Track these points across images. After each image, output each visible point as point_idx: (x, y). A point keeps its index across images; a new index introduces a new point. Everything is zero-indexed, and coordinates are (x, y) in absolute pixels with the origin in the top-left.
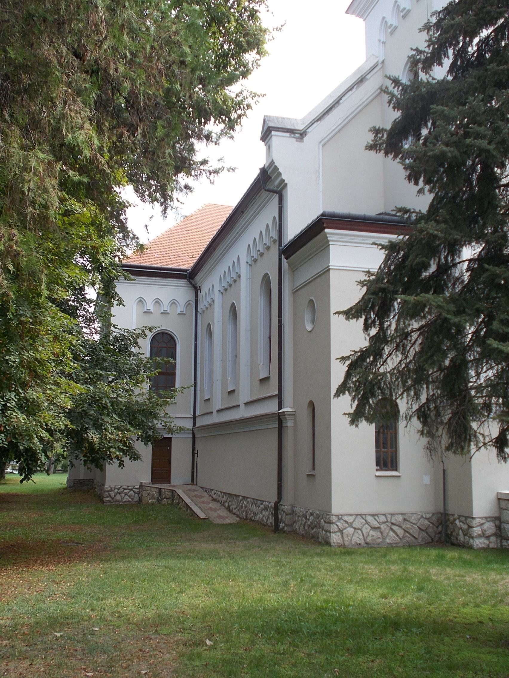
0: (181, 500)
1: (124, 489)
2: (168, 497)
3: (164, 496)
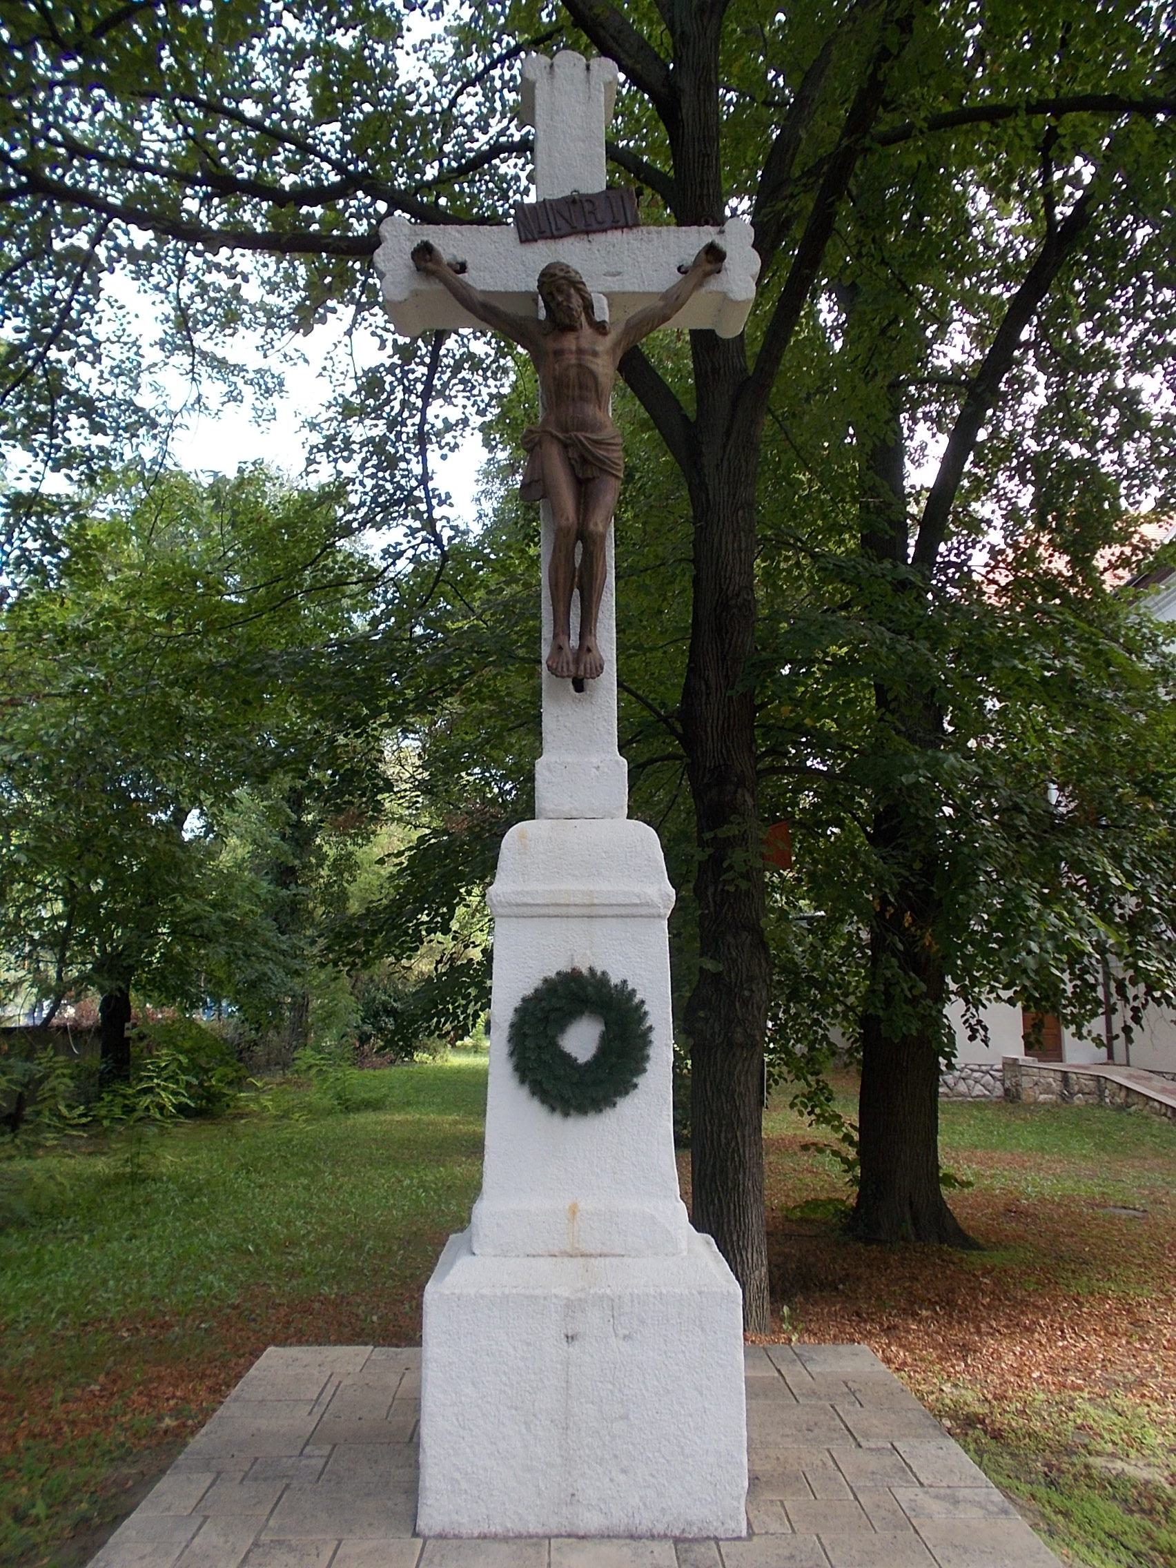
0: (1134, 1098)
1: (973, 1070)
2: (1087, 1090)
3: (1076, 1088)
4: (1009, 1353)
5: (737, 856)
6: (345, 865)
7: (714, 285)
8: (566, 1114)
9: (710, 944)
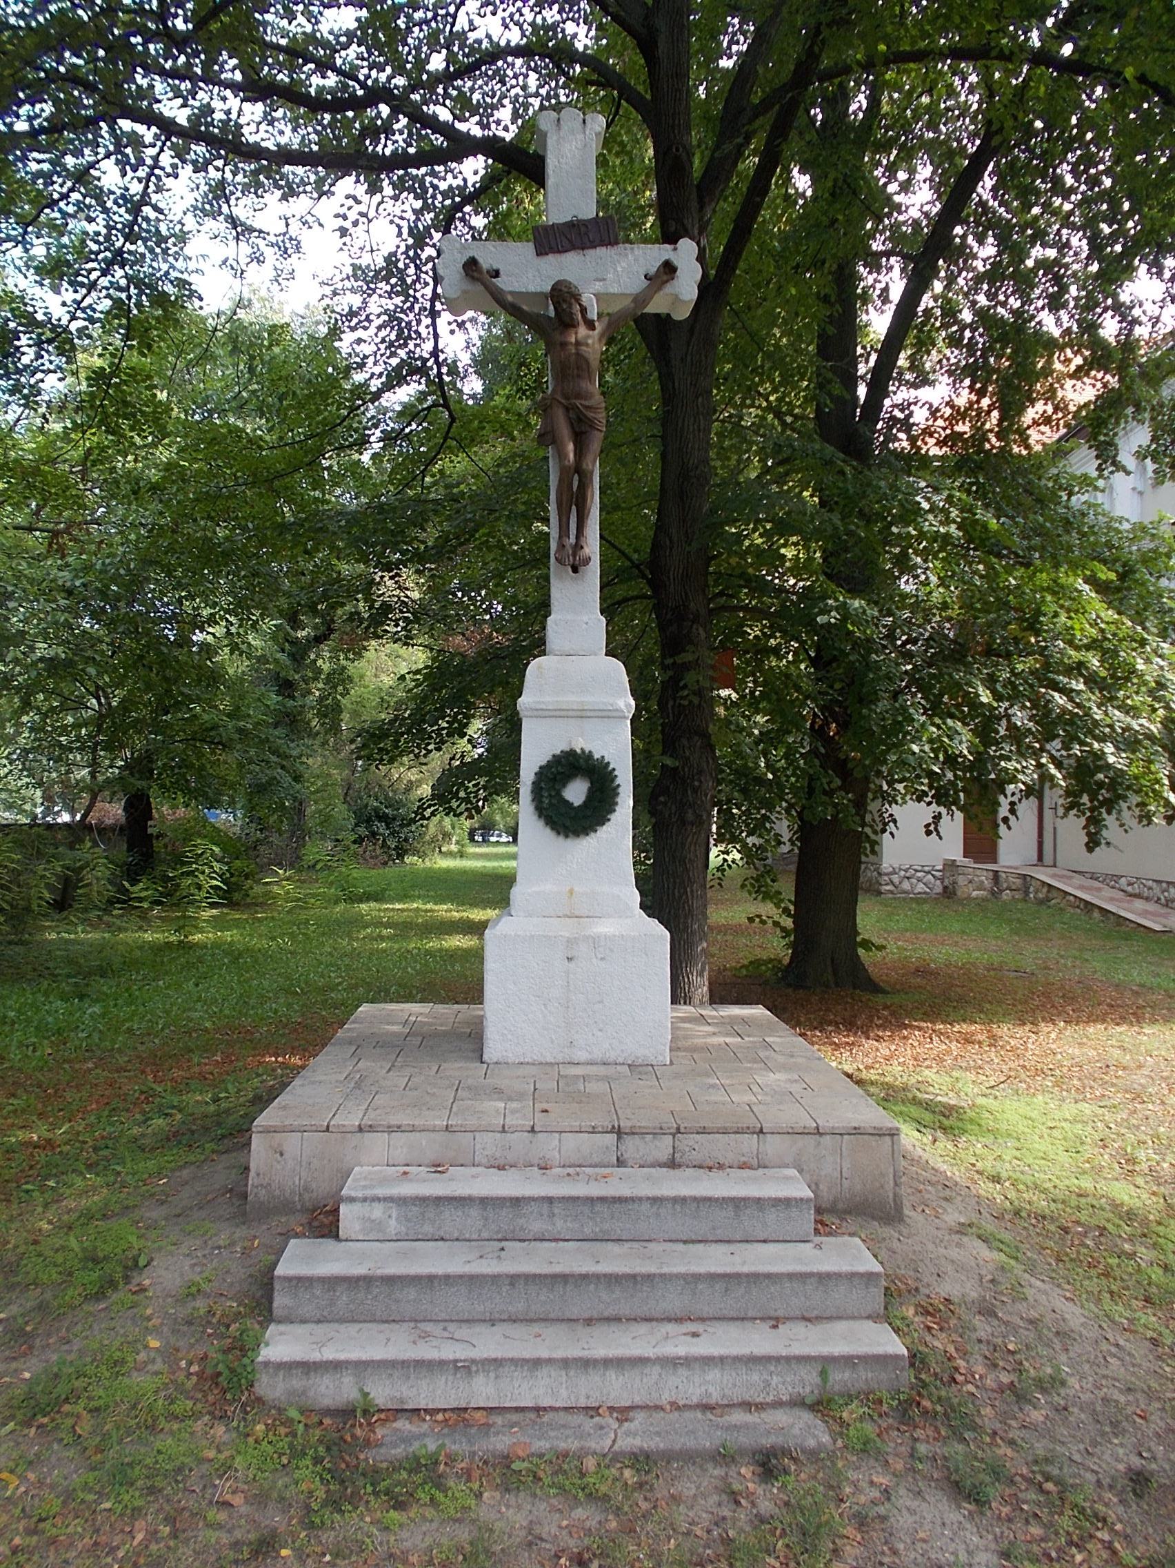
4: (884, 1049)
5: (690, 678)
6: (339, 679)
7: (669, 289)
8: (567, 836)
9: (669, 746)
